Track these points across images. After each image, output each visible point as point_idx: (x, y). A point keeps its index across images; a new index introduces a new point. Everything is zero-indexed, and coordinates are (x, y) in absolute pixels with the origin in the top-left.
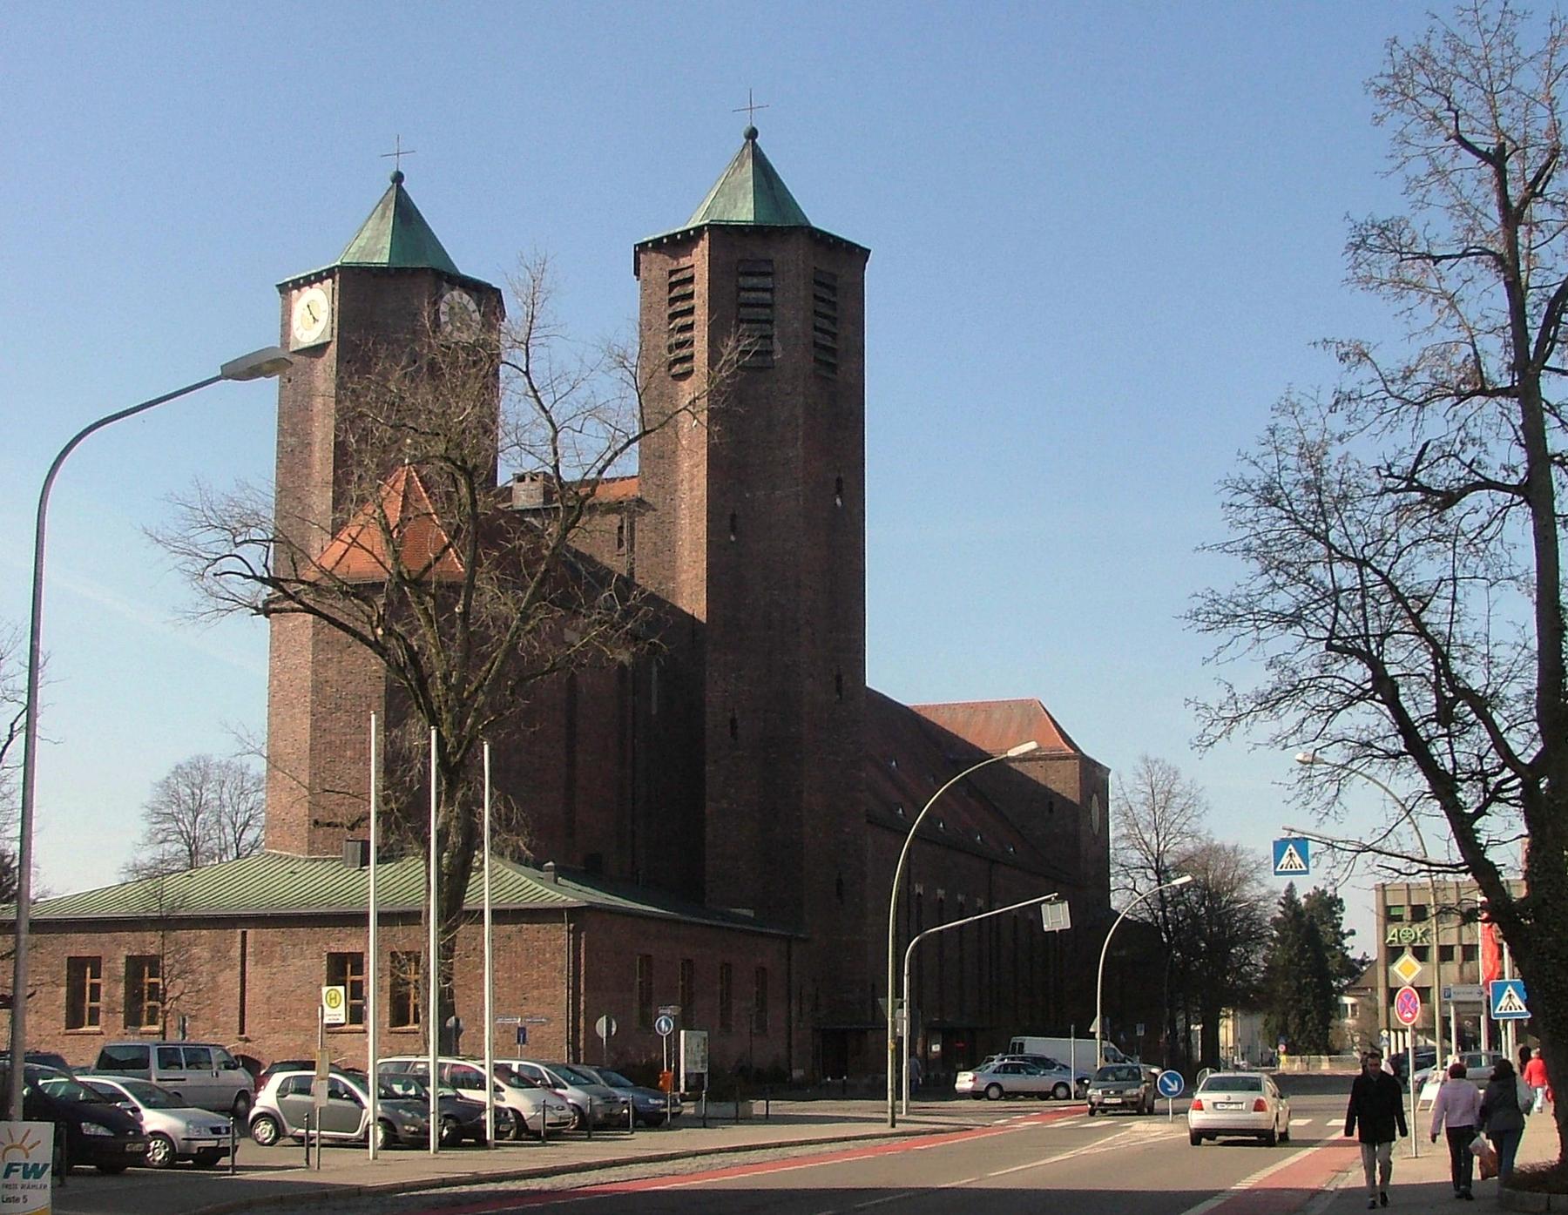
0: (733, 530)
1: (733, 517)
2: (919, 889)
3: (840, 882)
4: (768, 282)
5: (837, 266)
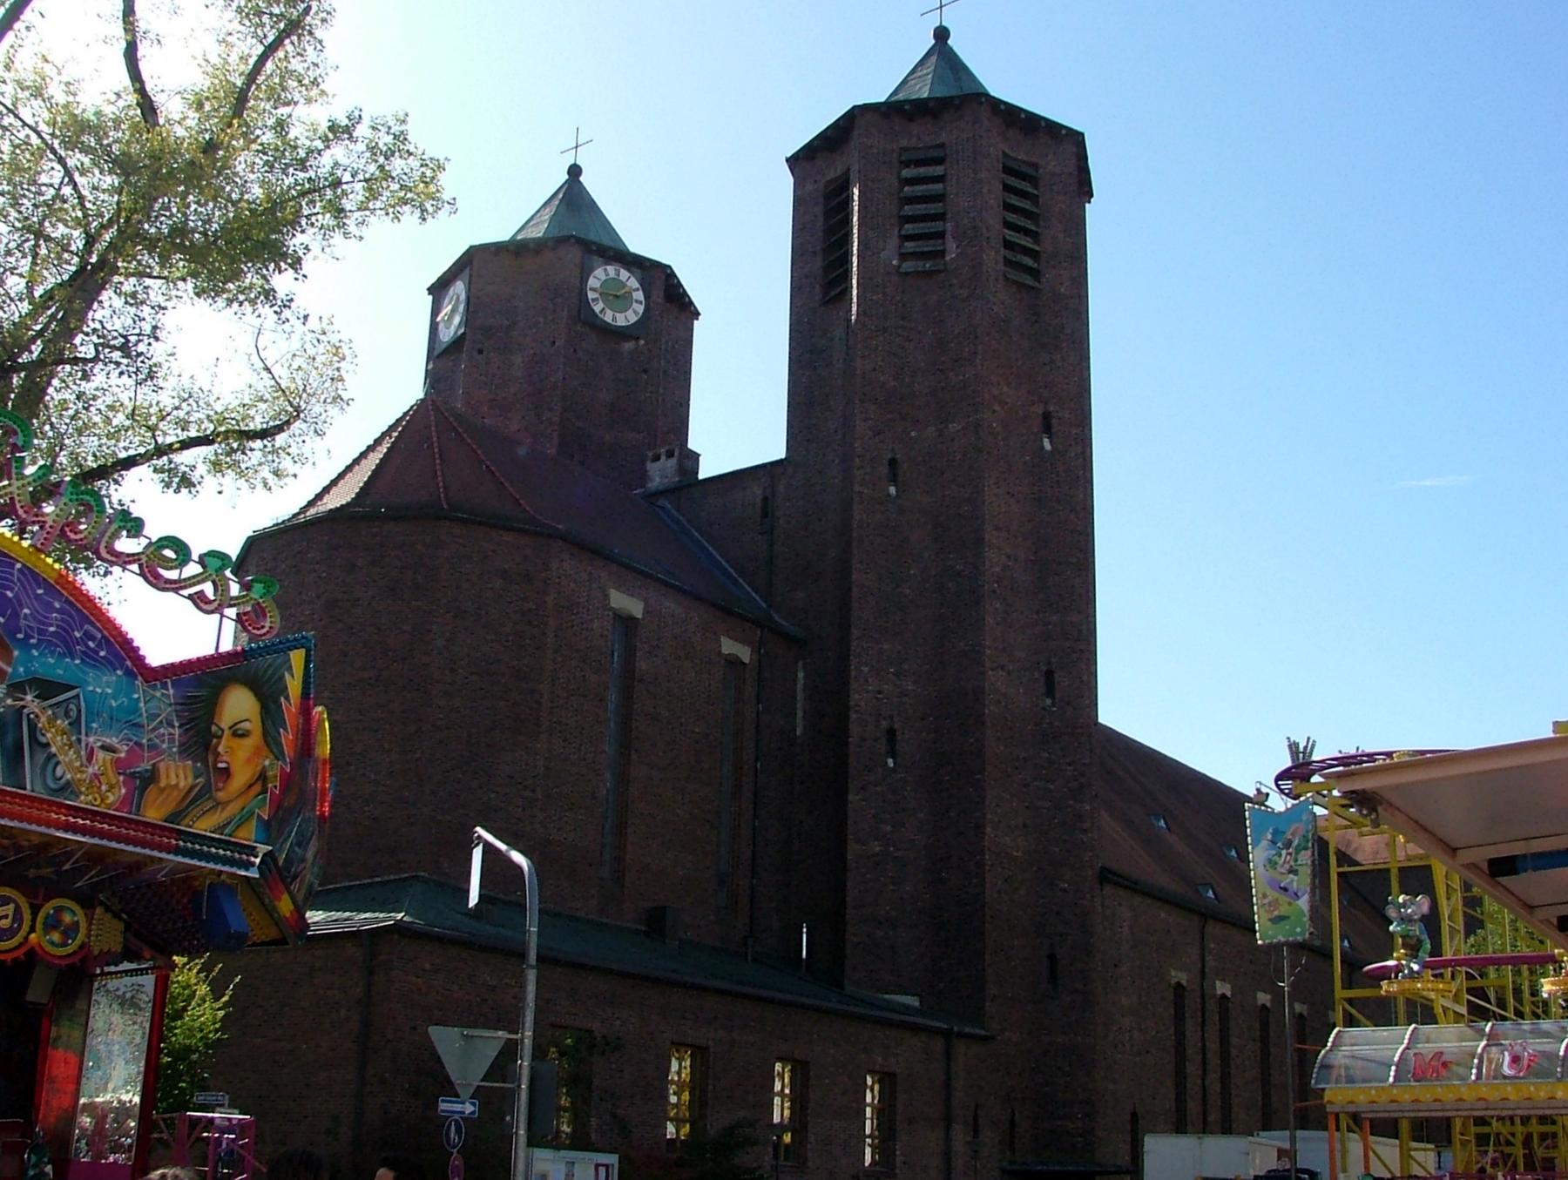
0: (894, 479)
1: (893, 463)
2: (1223, 988)
3: (1052, 958)
4: (938, 170)
5: (1040, 171)
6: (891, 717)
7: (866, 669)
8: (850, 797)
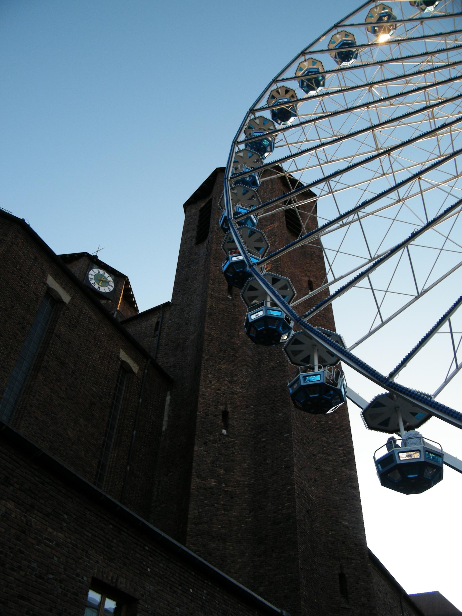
3: (342, 576)
6: (226, 404)
7: (211, 376)
8: (196, 448)
